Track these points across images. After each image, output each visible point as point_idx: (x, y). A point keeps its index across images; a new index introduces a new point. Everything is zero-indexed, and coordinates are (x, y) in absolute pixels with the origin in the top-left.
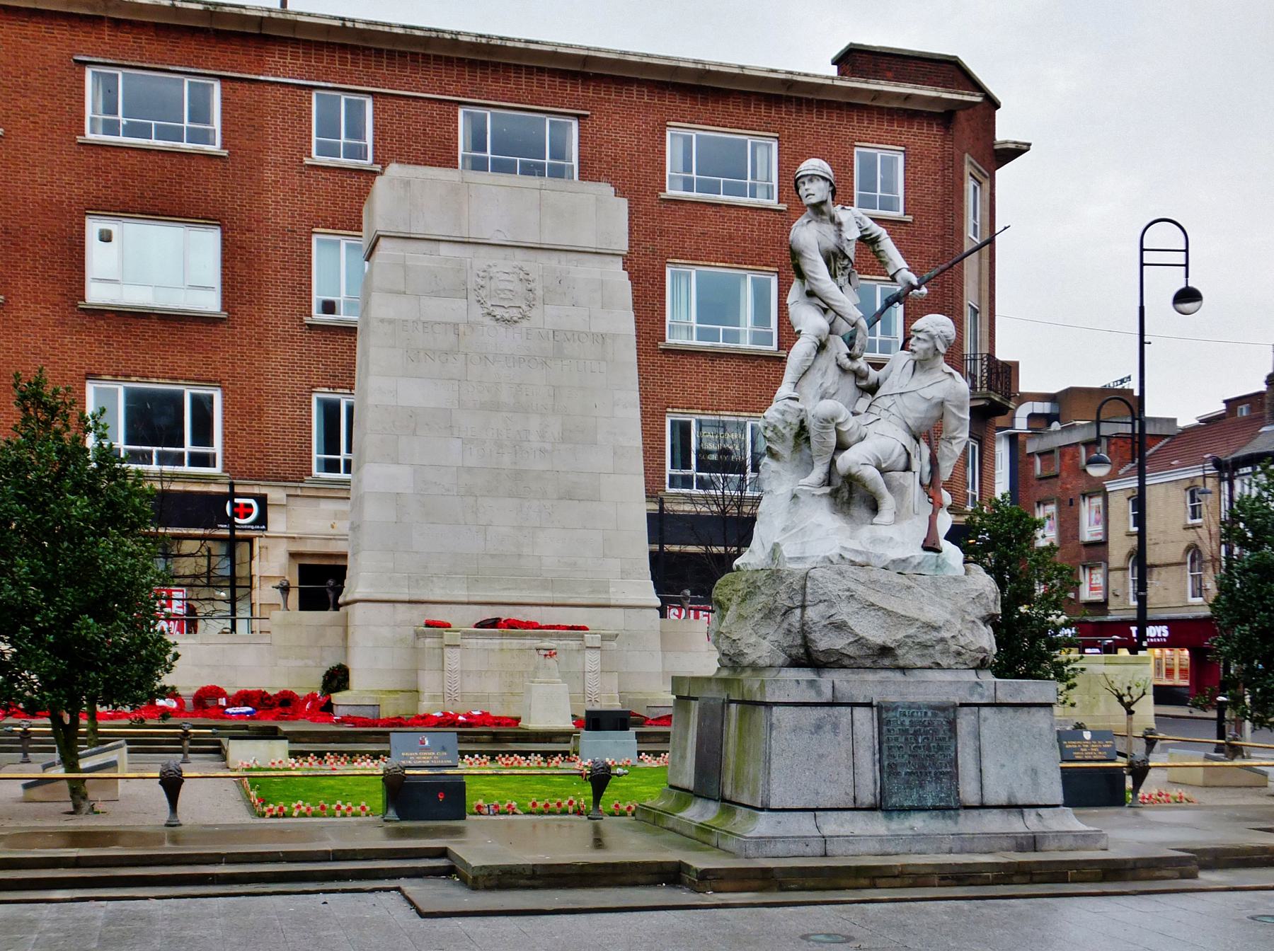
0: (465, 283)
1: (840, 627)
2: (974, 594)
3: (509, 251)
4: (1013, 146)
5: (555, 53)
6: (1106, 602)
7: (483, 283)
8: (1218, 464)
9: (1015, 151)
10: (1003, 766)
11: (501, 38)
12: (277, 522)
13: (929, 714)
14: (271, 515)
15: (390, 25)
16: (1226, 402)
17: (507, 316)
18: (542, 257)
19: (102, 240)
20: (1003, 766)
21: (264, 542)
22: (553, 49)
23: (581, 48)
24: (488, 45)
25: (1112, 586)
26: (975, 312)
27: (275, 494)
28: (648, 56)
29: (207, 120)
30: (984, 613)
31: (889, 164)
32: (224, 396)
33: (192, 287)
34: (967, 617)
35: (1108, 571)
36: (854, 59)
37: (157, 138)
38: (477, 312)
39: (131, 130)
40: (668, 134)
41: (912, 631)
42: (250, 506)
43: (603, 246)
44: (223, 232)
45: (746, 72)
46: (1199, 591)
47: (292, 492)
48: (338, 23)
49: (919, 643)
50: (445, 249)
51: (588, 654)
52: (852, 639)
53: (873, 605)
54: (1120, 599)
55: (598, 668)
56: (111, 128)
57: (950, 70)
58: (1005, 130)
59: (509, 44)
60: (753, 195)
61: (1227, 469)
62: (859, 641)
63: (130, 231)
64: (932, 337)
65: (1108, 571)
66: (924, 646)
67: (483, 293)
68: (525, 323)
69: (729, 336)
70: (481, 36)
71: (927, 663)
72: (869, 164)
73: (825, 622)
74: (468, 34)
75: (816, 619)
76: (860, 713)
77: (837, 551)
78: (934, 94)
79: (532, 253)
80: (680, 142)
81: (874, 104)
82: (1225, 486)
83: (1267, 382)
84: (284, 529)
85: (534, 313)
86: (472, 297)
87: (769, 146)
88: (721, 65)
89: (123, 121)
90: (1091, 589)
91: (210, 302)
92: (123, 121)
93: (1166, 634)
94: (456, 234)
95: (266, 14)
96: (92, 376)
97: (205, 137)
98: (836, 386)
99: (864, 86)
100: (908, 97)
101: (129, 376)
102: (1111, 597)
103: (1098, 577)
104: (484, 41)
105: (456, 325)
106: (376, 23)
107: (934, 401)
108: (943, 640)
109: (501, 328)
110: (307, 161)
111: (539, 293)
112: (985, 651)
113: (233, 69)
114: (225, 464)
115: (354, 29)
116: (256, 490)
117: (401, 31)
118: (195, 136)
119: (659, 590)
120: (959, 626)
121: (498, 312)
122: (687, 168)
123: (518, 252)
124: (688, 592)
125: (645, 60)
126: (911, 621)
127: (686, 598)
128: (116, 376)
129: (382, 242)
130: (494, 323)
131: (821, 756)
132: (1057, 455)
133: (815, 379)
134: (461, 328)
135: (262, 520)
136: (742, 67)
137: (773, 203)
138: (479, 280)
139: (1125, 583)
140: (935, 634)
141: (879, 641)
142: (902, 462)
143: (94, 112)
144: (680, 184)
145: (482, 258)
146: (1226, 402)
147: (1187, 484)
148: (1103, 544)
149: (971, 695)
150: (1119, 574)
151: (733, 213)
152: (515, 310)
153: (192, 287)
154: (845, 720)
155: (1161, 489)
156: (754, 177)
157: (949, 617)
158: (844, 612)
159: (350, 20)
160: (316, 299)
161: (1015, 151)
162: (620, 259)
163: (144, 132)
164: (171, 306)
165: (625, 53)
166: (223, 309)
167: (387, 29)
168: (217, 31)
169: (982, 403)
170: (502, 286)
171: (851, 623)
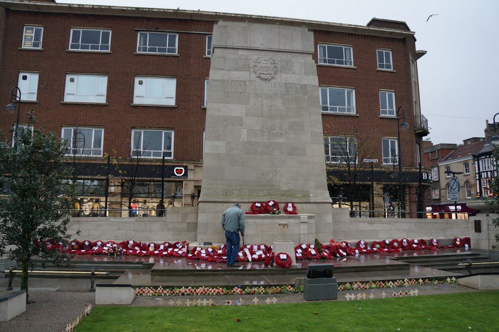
0: (249, 65)
3: (266, 52)
4: (421, 52)
5: (282, 20)
6: (440, 199)
7: (256, 65)
8: (474, 156)
9: (422, 54)
11: (265, 17)
12: (191, 176)
14: (189, 173)
15: (231, 14)
16: (464, 141)
17: (266, 78)
18: (280, 55)
19: (139, 84)
21: (186, 182)
23: (290, 19)
25: (442, 194)
26: (415, 102)
27: (191, 167)
28: (311, 21)
29: (174, 46)
31: (387, 55)
32: (175, 133)
33: (167, 98)
35: (440, 189)
36: (374, 22)
37: (108, 43)
38: (253, 77)
39: (150, 50)
40: (318, 46)
42: (182, 170)
43: (304, 50)
44: (177, 80)
45: (342, 25)
46: (125, 215)
47: (196, 165)
48: (214, 14)
50: (240, 52)
51: (302, 226)
54: (445, 198)
55: (306, 232)
56: (145, 49)
57: (403, 25)
58: (419, 47)
59: (268, 18)
60: (346, 64)
61: (477, 157)
63: (147, 81)
65: (440, 189)
67: (256, 68)
68: (273, 81)
69: (340, 109)
70: (259, 16)
72: (381, 54)
74: (254, 16)
78: (400, 32)
79: (276, 53)
80: (322, 48)
81: (382, 36)
82: (476, 162)
83: (486, 131)
84: (193, 178)
85: (277, 76)
86: (252, 70)
87: (350, 49)
88: (334, 23)
89: (148, 47)
90: (435, 195)
91: (172, 102)
92: (148, 47)
93: (431, 209)
94: (245, 45)
95: (192, 12)
96: (133, 128)
97: (174, 51)
99: (379, 29)
100: (392, 33)
101: (145, 127)
102: (442, 198)
103: (437, 192)
105: (245, 82)
106: (226, 13)
109: (263, 83)
110: (204, 57)
111: (279, 68)
113: (182, 30)
114: (174, 156)
115: (219, 15)
116: (184, 165)
117: (234, 15)
118: (169, 51)
119: (331, 195)
121: (262, 76)
122: (325, 56)
123: (270, 53)
125: (310, 22)
127: (340, 198)
128: (141, 128)
129: (215, 49)
130: (260, 81)
132: (437, 151)
134: (247, 83)
135: (186, 175)
136: (341, 24)
137: (352, 66)
138: (254, 63)
139: (446, 193)
143: (140, 45)
144: (323, 61)
145: (254, 56)
146: (464, 141)
147: (446, 166)
148: (438, 181)
150: (444, 190)
151: (340, 69)
152: (269, 75)
153: (167, 98)
155: (456, 165)
156: (346, 58)
159: (218, 13)
160: (144, 80)
161: (422, 54)
163: (154, 50)
164: (160, 104)
165: (304, 20)
166: (176, 104)
167: (230, 15)
168: (178, 19)
169: (421, 131)
170: (264, 65)
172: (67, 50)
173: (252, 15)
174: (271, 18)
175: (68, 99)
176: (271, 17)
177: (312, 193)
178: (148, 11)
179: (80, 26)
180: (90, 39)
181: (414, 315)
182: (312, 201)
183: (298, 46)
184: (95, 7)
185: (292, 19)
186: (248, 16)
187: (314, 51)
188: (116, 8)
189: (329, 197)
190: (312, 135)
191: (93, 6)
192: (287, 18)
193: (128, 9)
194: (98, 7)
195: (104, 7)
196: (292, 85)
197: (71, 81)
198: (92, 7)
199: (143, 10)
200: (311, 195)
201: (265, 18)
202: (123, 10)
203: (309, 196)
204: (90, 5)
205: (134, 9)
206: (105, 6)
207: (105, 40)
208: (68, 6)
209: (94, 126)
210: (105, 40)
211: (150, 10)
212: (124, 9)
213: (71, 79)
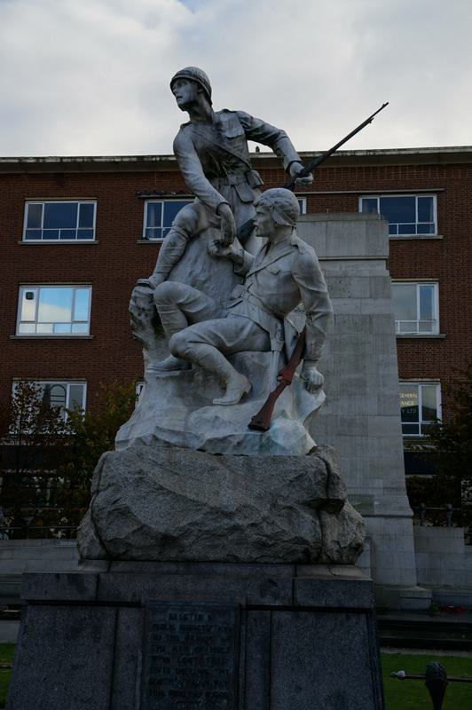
1: (125, 513)
2: (293, 476)
5: (418, 154)
10: (299, 689)
13: (206, 618)
15: (314, 153)
20: (299, 689)
22: (416, 152)
24: (374, 156)
30: (306, 497)
34: (280, 502)
37: (92, 226)
41: (198, 518)
49: (207, 532)
52: (136, 527)
53: (161, 488)
59: (387, 153)
62: (142, 529)
64: (267, 209)
66: (213, 535)
70: (370, 151)
71: (221, 555)
73: (110, 508)
75: (102, 505)
76: (127, 616)
77: (152, 431)
98: (207, 274)
104: (371, 154)
107: (282, 275)
108: (236, 528)
112: (305, 542)
119: (412, 505)
120: (265, 513)
124: (450, 506)
126: (198, 505)
131: (75, 667)
133: (184, 269)
140: (226, 521)
141: (162, 529)
142: (259, 340)
149: (262, 596)
154: (109, 623)
157: (251, 502)
158: (127, 498)
160: (34, 290)
162: (385, 262)
171: (134, 509)
172: (19, 242)
173: (355, 151)
174: (394, 153)
175: (24, 330)
176: (394, 150)
177: (378, 500)
178: (160, 161)
179: (43, 195)
180: (59, 218)
181: (144, 700)
182: (376, 512)
183: (360, 250)
184: (64, 160)
185: (439, 148)
186: (349, 154)
187: (388, 254)
188: (103, 160)
189: (408, 506)
190: (379, 400)
191: (62, 158)
192: (428, 149)
193: (125, 160)
194: (70, 160)
195: (81, 160)
196: (346, 318)
197: (27, 298)
198: (59, 161)
199: (150, 159)
200: (376, 503)
201: (381, 153)
202: (114, 162)
203: (372, 505)
204: (56, 158)
205: (135, 159)
206: (83, 158)
207: (86, 221)
208: (17, 161)
209: (68, 378)
210: (86, 221)
211: (164, 159)
212: (117, 160)
213: (27, 293)
